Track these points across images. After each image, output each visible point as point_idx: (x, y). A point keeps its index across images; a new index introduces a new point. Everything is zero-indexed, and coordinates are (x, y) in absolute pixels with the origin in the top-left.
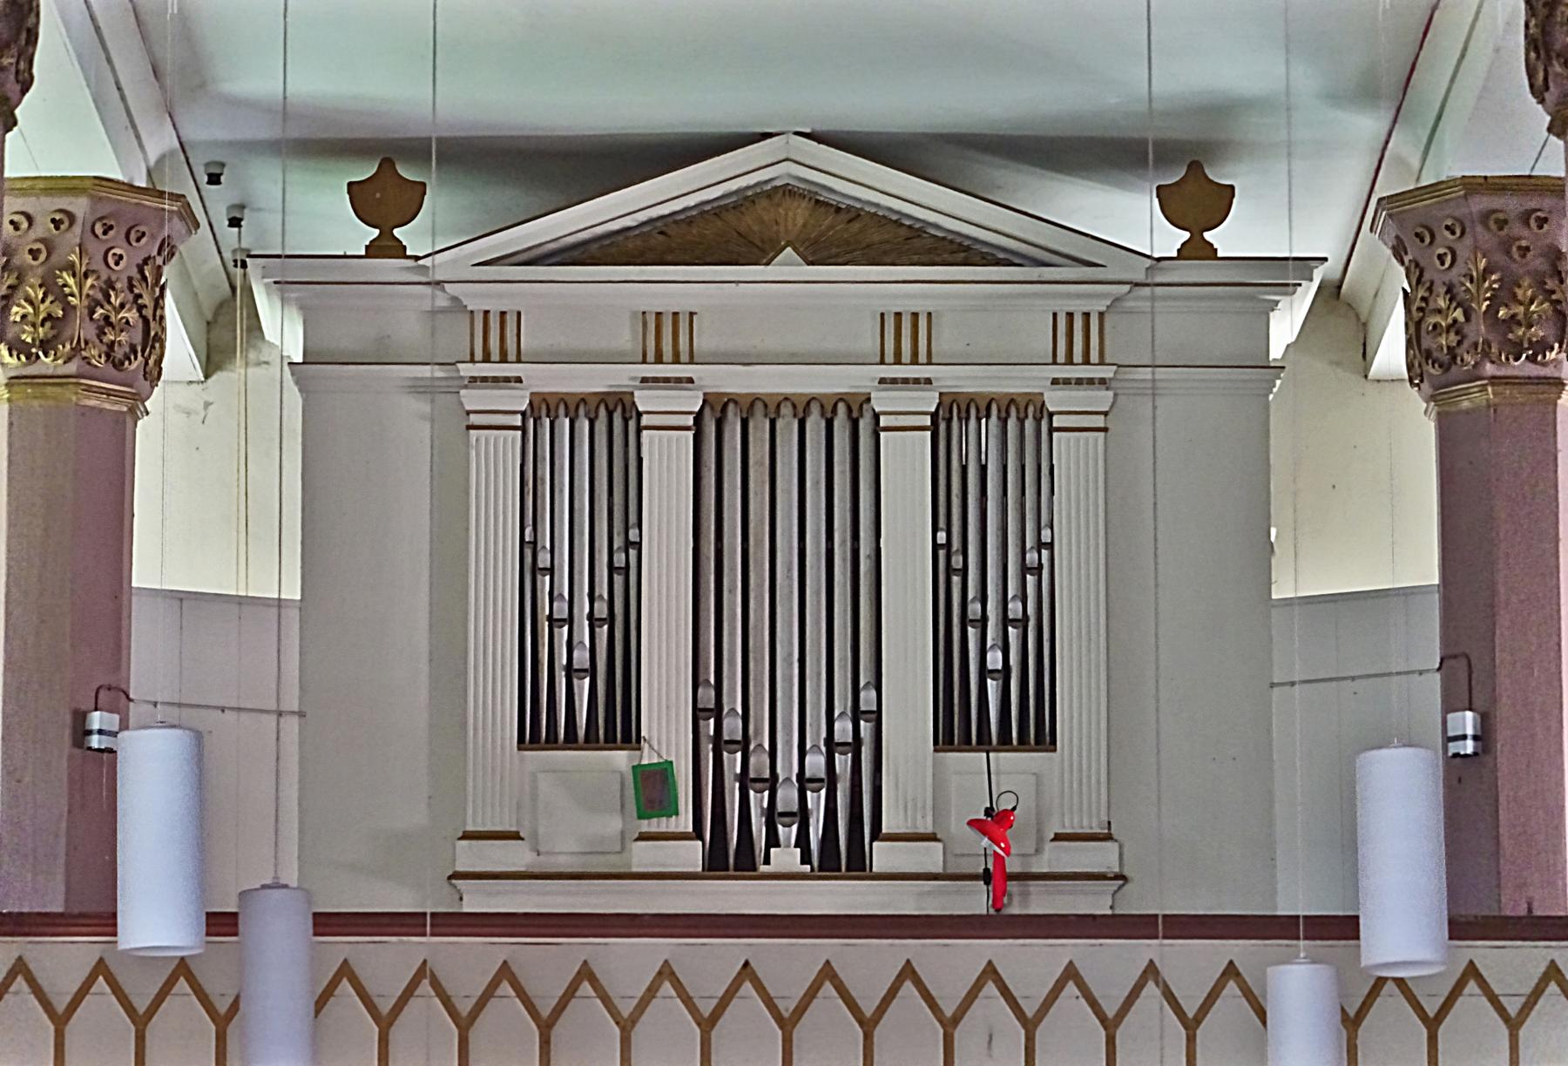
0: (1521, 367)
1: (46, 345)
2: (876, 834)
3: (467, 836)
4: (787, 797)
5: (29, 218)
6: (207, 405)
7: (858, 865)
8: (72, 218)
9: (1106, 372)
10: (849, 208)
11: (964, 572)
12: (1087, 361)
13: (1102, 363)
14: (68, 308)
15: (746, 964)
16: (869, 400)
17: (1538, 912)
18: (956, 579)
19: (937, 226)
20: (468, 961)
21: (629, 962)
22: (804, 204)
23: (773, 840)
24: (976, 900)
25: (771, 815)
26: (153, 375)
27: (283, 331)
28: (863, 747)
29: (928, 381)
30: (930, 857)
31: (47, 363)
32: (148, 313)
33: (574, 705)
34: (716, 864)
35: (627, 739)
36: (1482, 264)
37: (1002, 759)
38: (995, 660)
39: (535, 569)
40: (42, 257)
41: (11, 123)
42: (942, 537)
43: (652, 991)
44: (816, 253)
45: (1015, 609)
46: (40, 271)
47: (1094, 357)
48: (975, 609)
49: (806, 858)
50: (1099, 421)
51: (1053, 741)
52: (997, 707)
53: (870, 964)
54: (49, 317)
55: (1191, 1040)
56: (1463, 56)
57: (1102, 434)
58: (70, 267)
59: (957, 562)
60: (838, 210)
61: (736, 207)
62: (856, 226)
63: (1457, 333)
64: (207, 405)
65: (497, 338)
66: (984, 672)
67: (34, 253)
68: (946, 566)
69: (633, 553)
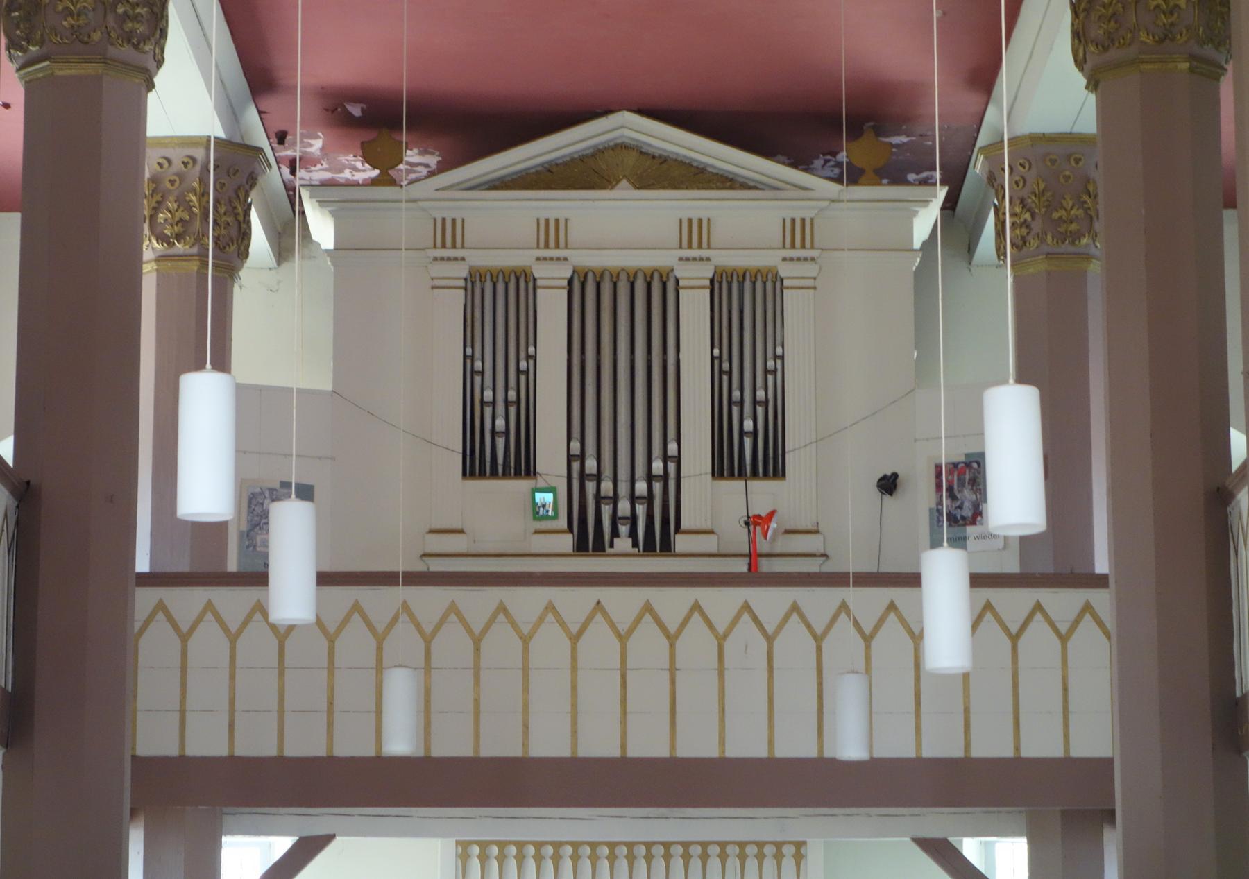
0: (1066, 247)
1: (179, 237)
2: (678, 529)
3: (432, 531)
4: (624, 507)
5: (169, 161)
6: (279, 282)
7: (667, 547)
8: (194, 160)
9: (814, 253)
10: (660, 156)
11: (730, 373)
12: (803, 247)
13: (812, 247)
14: (192, 214)
15: (599, 603)
16: (672, 270)
17: (1077, 571)
18: (725, 378)
19: (712, 166)
20: (430, 600)
21: (527, 601)
22: (634, 154)
23: (615, 533)
24: (741, 566)
25: (615, 519)
26: (244, 254)
27: (322, 228)
28: (671, 481)
29: (708, 259)
30: (708, 544)
31: (180, 247)
32: (241, 218)
33: (497, 450)
34: (581, 547)
35: (528, 474)
36: (1042, 186)
37: (755, 485)
38: (748, 425)
39: (473, 372)
40: (177, 184)
41: (150, 86)
42: (716, 352)
43: (541, 619)
44: (643, 182)
45: (760, 394)
46: (176, 193)
47: (808, 243)
48: (736, 394)
49: (635, 544)
50: (810, 283)
51: (784, 475)
52: (749, 451)
53: (671, 602)
54: (181, 220)
55: (868, 648)
56: (1030, 57)
57: (812, 291)
58: (194, 191)
59: (726, 366)
60: (654, 157)
61: (593, 155)
62: (665, 166)
63: (1116, 22)
64: (279, 282)
65: (448, 234)
66: (742, 433)
67: (172, 182)
68: (719, 372)
69: (531, 362)
